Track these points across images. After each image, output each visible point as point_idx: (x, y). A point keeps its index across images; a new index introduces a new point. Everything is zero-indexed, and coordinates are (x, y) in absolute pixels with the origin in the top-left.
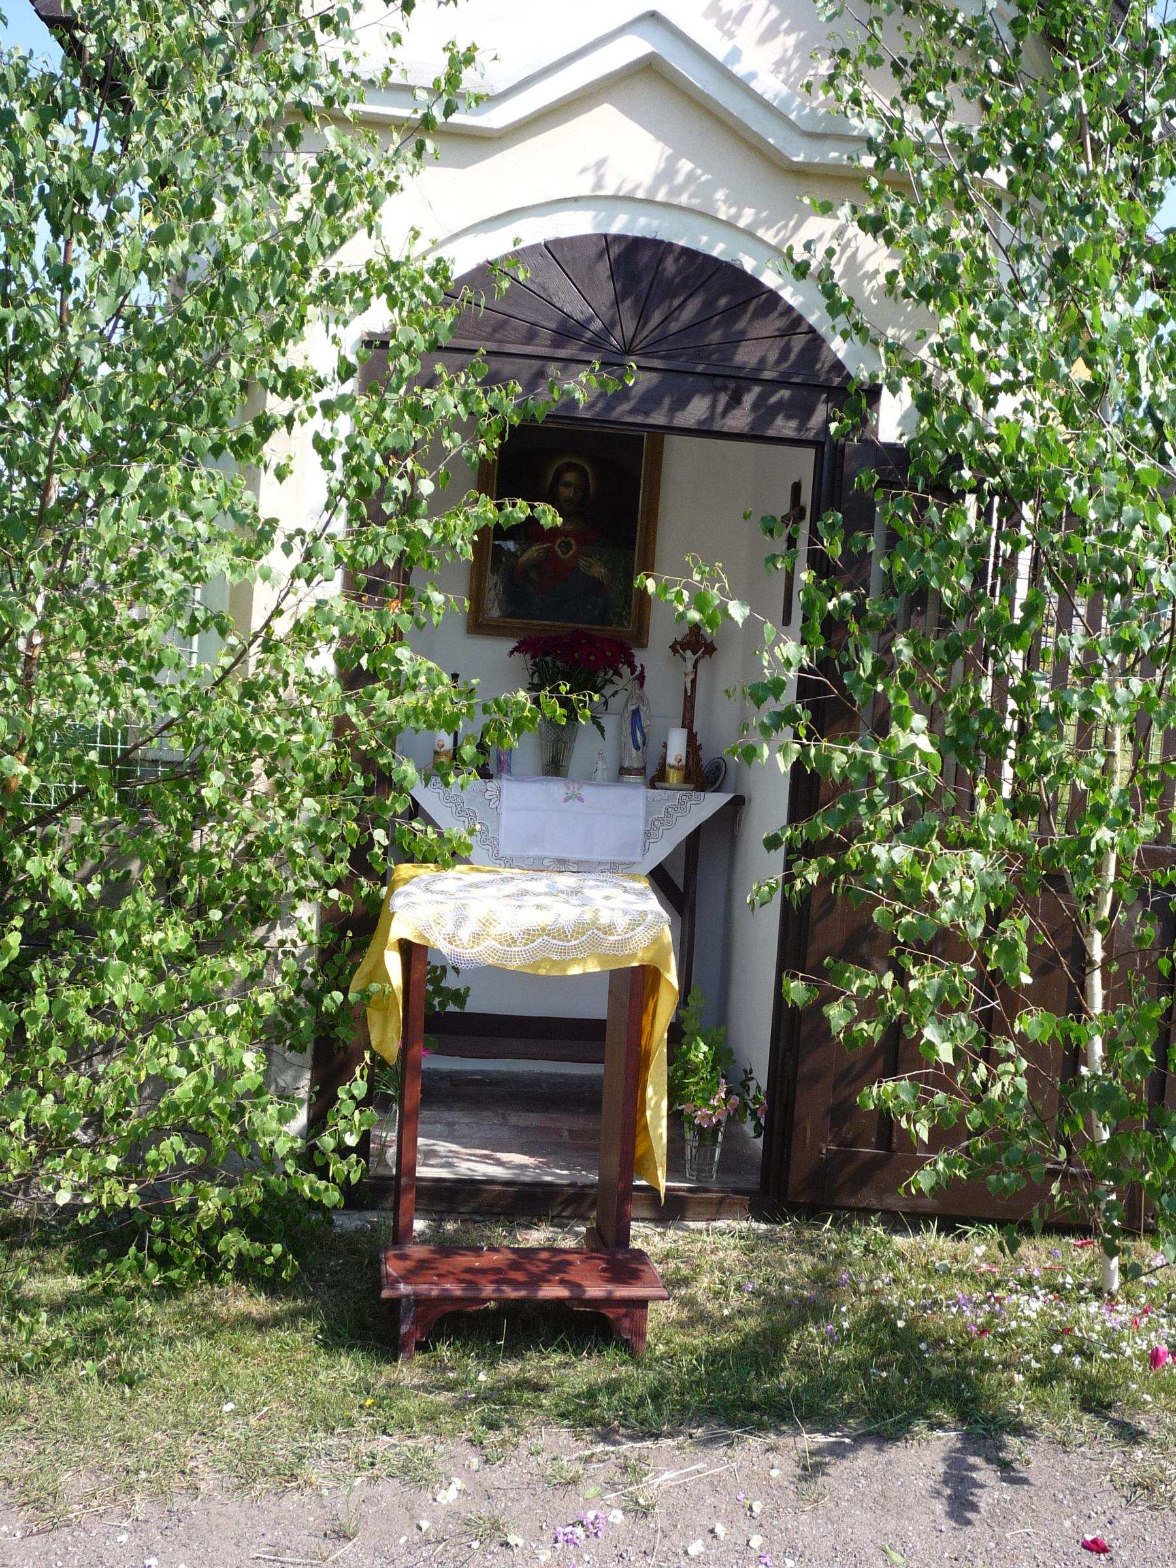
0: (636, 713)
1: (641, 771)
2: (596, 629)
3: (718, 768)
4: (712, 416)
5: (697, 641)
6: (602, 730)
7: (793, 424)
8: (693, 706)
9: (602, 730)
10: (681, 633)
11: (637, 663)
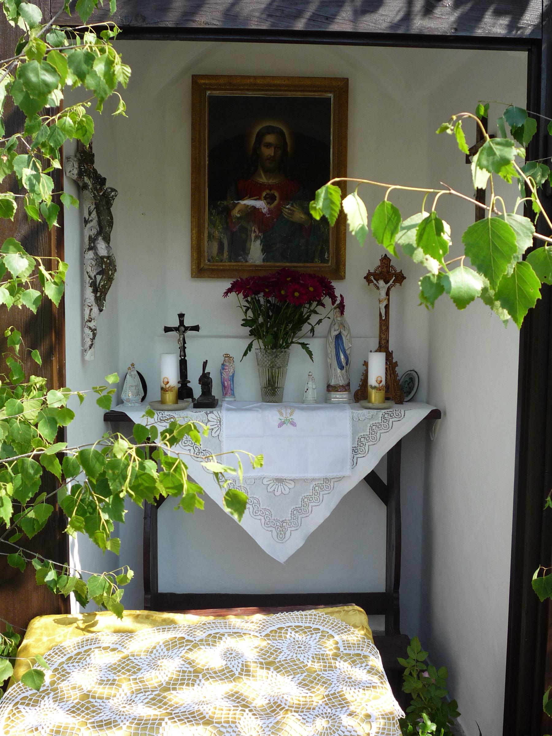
0: (338, 337)
1: (346, 388)
2: (301, 267)
3: (412, 379)
4: (407, 17)
5: (388, 272)
6: (310, 354)
7: (504, 21)
8: (388, 328)
9: (310, 354)
10: (374, 264)
11: (337, 293)
